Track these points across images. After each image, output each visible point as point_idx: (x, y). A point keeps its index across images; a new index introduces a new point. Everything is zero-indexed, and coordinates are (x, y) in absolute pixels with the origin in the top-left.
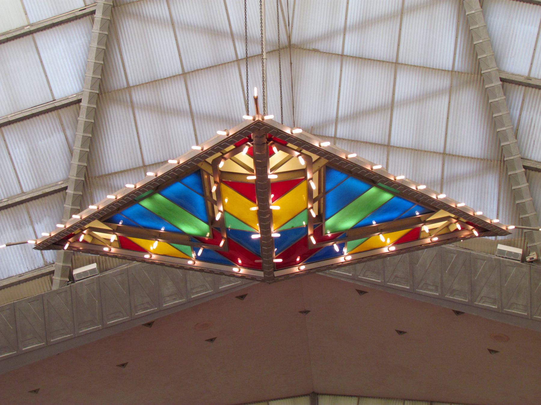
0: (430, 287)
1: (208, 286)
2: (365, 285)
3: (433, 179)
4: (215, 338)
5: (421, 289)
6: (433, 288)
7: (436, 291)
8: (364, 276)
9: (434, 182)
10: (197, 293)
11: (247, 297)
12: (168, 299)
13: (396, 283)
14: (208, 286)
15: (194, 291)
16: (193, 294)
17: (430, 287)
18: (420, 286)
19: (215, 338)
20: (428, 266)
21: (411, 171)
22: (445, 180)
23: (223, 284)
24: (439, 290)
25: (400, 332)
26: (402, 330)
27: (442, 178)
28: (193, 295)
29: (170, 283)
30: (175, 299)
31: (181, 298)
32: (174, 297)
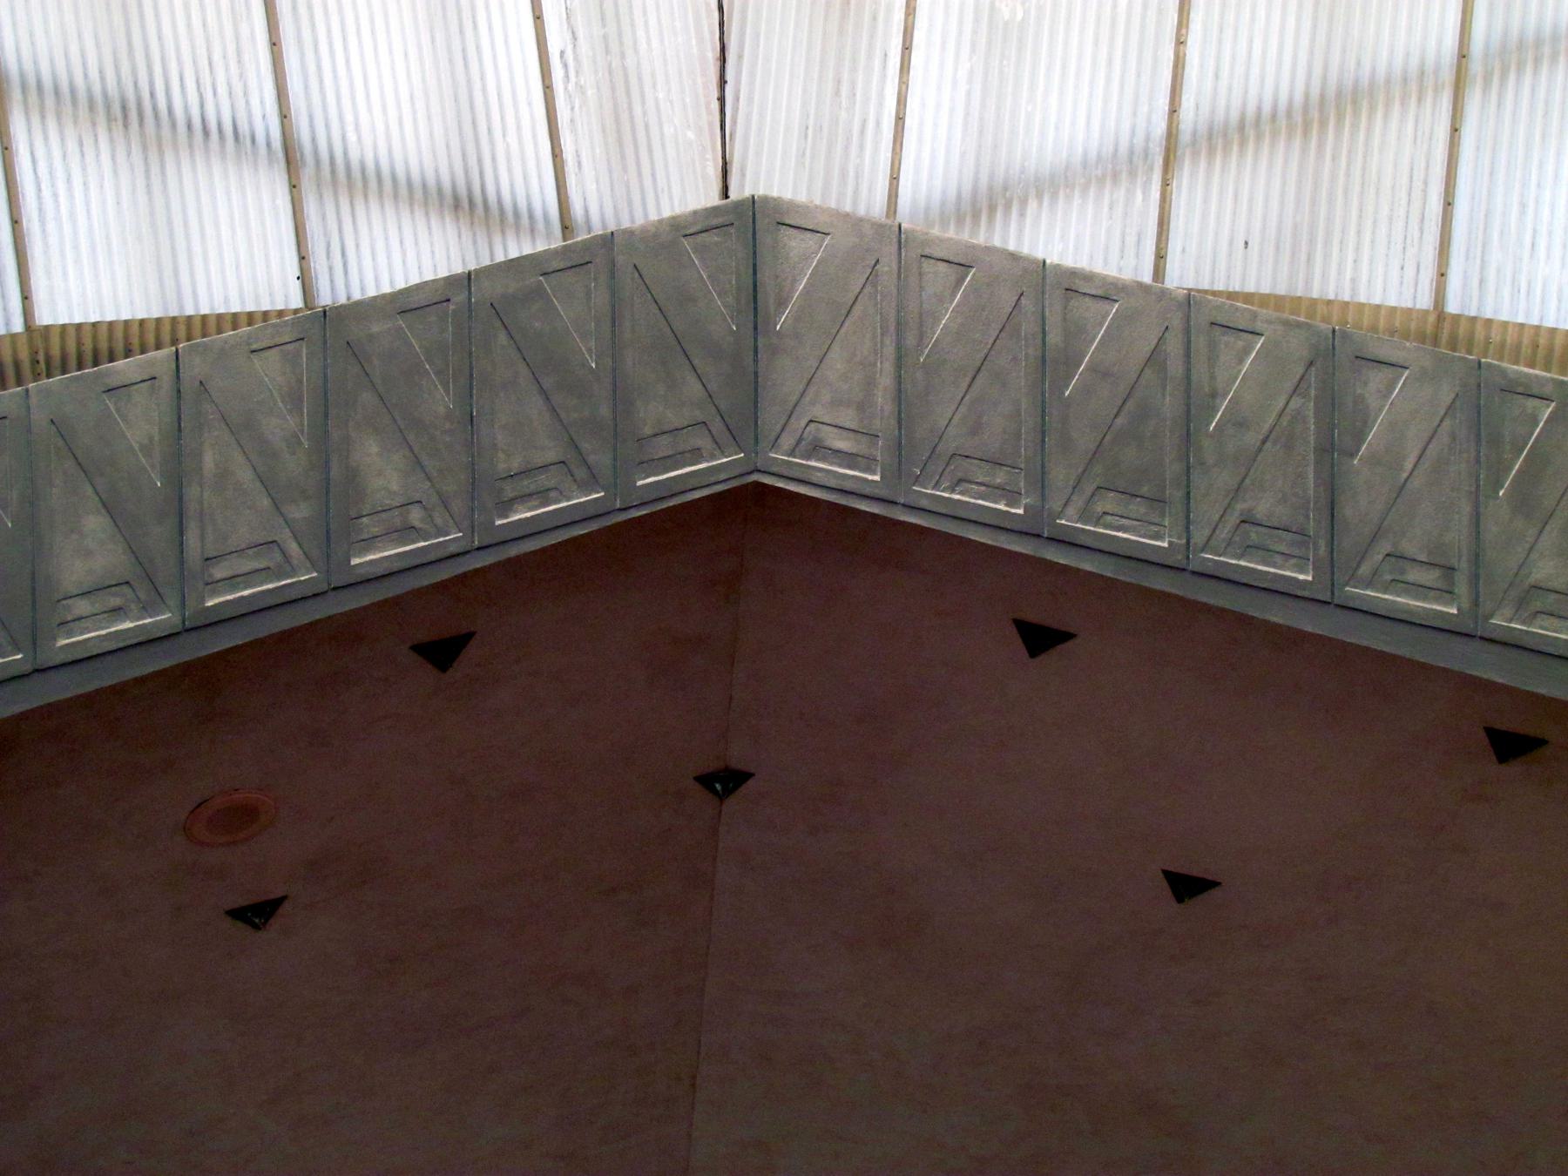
0: (1415, 575)
1: (293, 547)
2: (1087, 566)
3: (1414, 62)
4: (276, 903)
5: (1369, 584)
6: (1429, 577)
7: (1448, 593)
8: (1084, 516)
9: (1422, 73)
10: (233, 581)
11: (472, 652)
12: (82, 607)
13: (1248, 550)
14: (293, 547)
15: (219, 572)
16: (214, 586)
17: (1415, 575)
18: (1365, 570)
19: (276, 903)
20: (1409, 465)
21: (1307, 24)
22: (1476, 66)
23: (369, 543)
24: (1462, 588)
25: (1185, 886)
26: (1196, 871)
27: (1172, 135)
28: (214, 593)
29: (95, 523)
30: (117, 612)
31: (146, 609)
32: (115, 601)
